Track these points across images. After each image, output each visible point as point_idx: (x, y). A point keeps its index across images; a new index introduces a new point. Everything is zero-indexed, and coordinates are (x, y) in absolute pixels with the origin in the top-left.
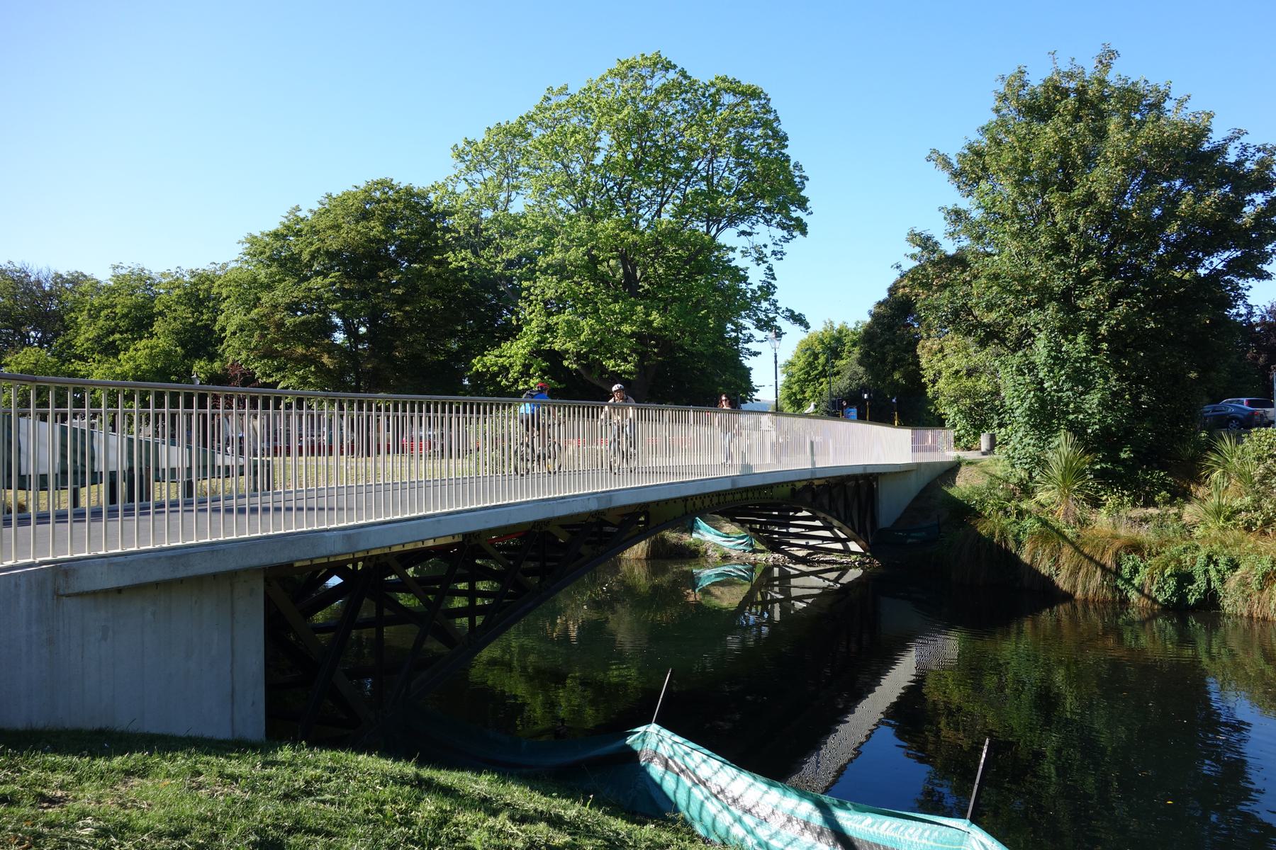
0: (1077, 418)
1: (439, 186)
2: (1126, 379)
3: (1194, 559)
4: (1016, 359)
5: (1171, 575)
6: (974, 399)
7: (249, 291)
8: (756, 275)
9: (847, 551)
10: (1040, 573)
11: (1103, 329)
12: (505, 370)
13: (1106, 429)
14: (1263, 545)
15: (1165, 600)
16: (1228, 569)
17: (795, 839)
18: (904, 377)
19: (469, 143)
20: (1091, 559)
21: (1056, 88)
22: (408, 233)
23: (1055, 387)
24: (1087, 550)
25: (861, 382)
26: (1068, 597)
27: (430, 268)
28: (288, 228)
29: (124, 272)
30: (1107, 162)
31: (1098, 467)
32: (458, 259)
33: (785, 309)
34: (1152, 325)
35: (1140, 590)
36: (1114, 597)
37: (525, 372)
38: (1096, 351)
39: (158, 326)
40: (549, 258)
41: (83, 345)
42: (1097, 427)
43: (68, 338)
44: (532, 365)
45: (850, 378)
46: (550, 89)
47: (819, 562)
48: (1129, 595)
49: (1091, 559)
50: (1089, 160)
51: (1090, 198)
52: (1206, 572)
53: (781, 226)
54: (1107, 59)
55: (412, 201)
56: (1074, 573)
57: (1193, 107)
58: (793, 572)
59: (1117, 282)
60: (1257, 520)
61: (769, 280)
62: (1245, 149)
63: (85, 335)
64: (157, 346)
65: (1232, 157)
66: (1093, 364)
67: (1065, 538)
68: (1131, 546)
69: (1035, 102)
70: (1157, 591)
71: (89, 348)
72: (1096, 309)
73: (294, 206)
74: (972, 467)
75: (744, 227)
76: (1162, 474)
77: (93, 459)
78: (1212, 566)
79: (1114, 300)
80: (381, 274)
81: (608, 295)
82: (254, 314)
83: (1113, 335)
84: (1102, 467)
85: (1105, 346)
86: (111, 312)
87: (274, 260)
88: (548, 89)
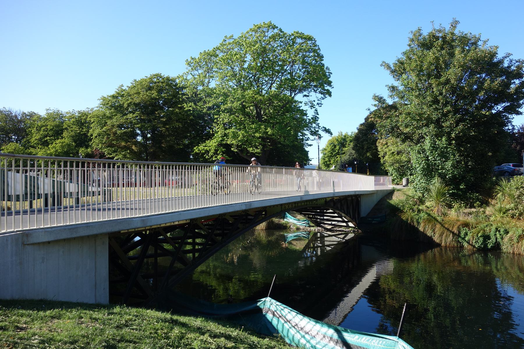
0: (442, 171)
1: (180, 76)
2: (463, 155)
3: (490, 229)
4: (417, 148)
5: (481, 236)
7: (102, 119)
8: (310, 113)
9: (348, 226)
10: (427, 235)
11: (453, 135)
12: (207, 152)
13: (454, 176)
14: (518, 224)
15: (478, 246)
16: (504, 234)
17: (326, 345)
18: (371, 155)
19: (193, 59)
20: (448, 229)
21: (434, 36)
22: (167, 96)
23: (433, 159)
24: (446, 226)
25: (354, 157)
26: (439, 245)
27: (177, 110)
28: (118, 94)
29: (51, 112)
30: (455, 66)
31: (451, 192)
32: (188, 106)
33: (322, 127)
34: (473, 133)
35: (468, 242)
36: (457, 245)
37: (216, 153)
38: (450, 144)
39: (65, 134)
40: (225, 106)
41: (34, 142)
42: (451, 175)
43: (28, 139)
44: (219, 150)
45: (349, 155)
46: (226, 37)
47: (336, 231)
48: (464, 244)
49: (448, 229)
50: (447, 66)
51: (448, 81)
52: (495, 235)
53: (321, 93)
54: (455, 24)
55: (169, 83)
56: (441, 235)
57: (490, 44)
58: (326, 235)
59: (459, 116)
60: (516, 213)
61: (316, 115)
62: (511, 61)
63: (35, 137)
64: (65, 142)
65: (506, 64)
66: (449, 150)
67: (437, 221)
68: (464, 224)
69: (425, 42)
70: (475, 243)
71: (36, 143)
72: (450, 127)
73: (121, 85)
74: (399, 192)
75: (305, 93)
76: (477, 195)
77: (38, 188)
78: (498, 232)
79: (457, 123)
80: (157, 113)
81: (250, 121)
82: (104, 129)
83: (457, 138)
84: (452, 192)
85: (454, 142)
86: (46, 128)
87: (113, 107)
88: (225, 37)
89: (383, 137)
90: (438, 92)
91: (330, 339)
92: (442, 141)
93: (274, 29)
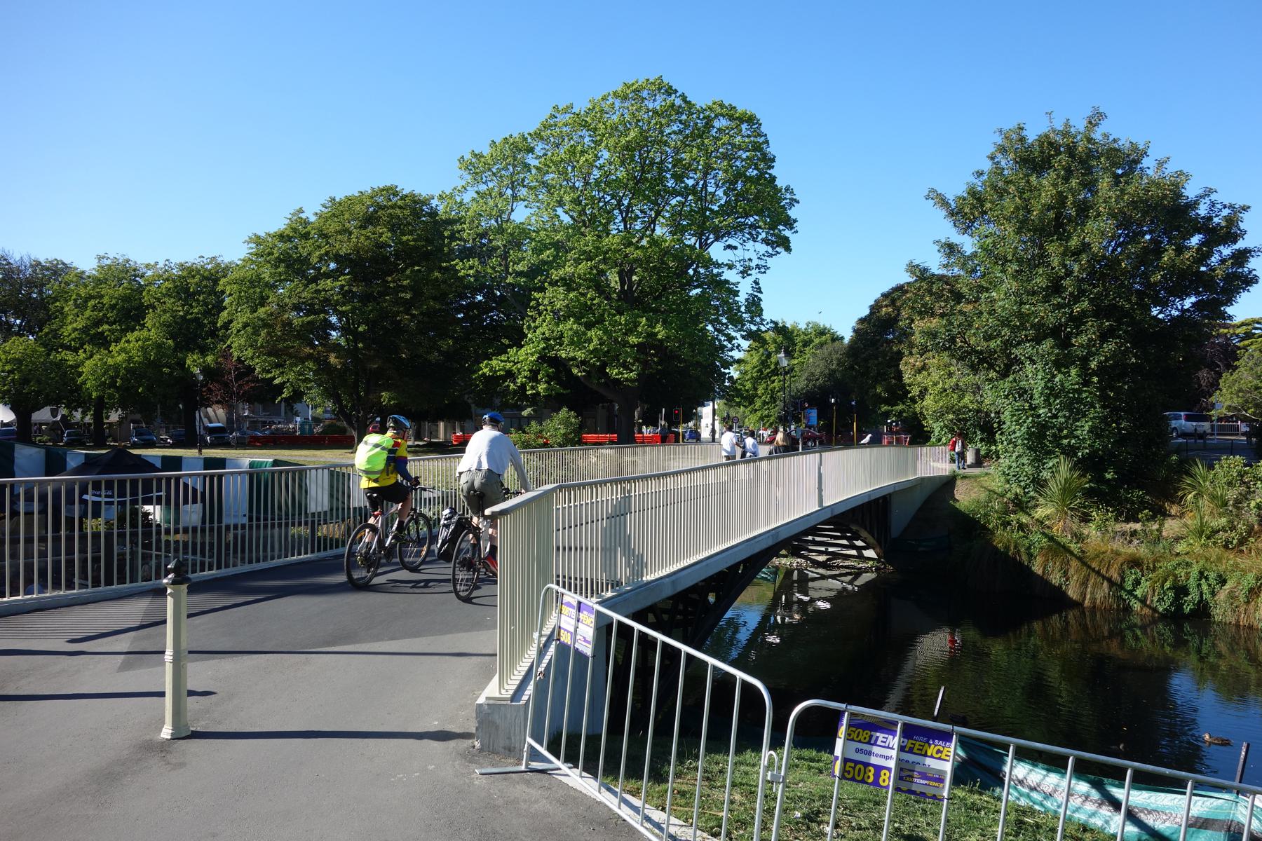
0: (1070, 442)
3: (1188, 574)
4: (1006, 385)
5: (1169, 588)
6: (958, 415)
7: (255, 289)
8: (745, 290)
9: (860, 557)
11: (1093, 365)
12: (510, 375)
13: (1093, 453)
14: (1244, 562)
16: (1217, 584)
18: (886, 390)
19: (476, 155)
20: (1098, 573)
21: (1051, 144)
22: (414, 240)
23: (1050, 414)
24: (1094, 565)
25: (818, 383)
26: (1077, 605)
27: (436, 274)
28: (295, 230)
29: (108, 262)
30: (1099, 215)
31: (1087, 486)
33: (769, 320)
35: (1143, 601)
36: (1118, 606)
37: (533, 376)
39: (149, 320)
40: (561, 272)
41: (70, 335)
42: (1087, 451)
43: (54, 327)
44: (539, 370)
47: (839, 567)
48: (1131, 604)
49: (1098, 573)
50: (1084, 209)
51: (1085, 247)
52: (1199, 585)
53: (766, 241)
55: (415, 205)
56: (1084, 583)
58: (811, 575)
59: (1107, 324)
60: (1233, 539)
61: (756, 294)
63: (71, 327)
64: (149, 339)
65: (1203, 210)
66: (1084, 395)
67: (1071, 553)
68: (1132, 562)
69: (1029, 155)
71: (76, 338)
72: (1088, 346)
73: (298, 208)
74: (966, 481)
76: (1141, 493)
77: (349, 497)
78: (1204, 580)
79: (1104, 336)
80: (390, 279)
81: (611, 306)
82: (262, 311)
83: (1102, 370)
84: (1090, 486)
85: (1095, 379)
86: (99, 303)
89: (915, 350)
90: (1063, 270)
91: (1084, 798)
92: (1069, 376)
93: (670, 95)
